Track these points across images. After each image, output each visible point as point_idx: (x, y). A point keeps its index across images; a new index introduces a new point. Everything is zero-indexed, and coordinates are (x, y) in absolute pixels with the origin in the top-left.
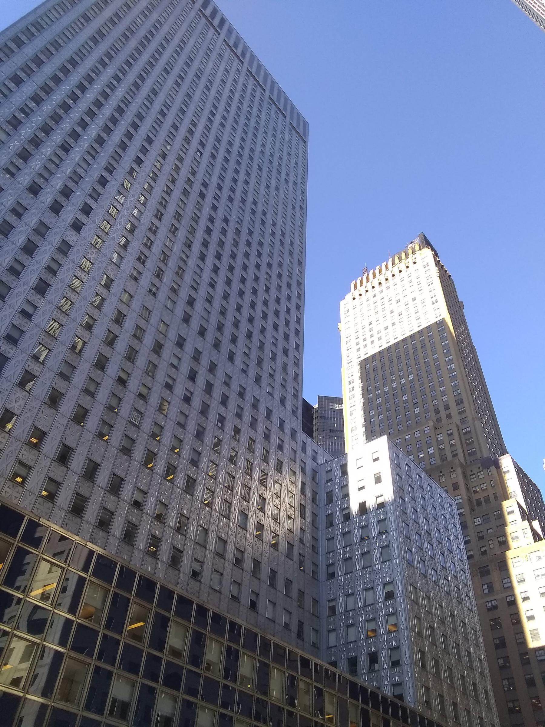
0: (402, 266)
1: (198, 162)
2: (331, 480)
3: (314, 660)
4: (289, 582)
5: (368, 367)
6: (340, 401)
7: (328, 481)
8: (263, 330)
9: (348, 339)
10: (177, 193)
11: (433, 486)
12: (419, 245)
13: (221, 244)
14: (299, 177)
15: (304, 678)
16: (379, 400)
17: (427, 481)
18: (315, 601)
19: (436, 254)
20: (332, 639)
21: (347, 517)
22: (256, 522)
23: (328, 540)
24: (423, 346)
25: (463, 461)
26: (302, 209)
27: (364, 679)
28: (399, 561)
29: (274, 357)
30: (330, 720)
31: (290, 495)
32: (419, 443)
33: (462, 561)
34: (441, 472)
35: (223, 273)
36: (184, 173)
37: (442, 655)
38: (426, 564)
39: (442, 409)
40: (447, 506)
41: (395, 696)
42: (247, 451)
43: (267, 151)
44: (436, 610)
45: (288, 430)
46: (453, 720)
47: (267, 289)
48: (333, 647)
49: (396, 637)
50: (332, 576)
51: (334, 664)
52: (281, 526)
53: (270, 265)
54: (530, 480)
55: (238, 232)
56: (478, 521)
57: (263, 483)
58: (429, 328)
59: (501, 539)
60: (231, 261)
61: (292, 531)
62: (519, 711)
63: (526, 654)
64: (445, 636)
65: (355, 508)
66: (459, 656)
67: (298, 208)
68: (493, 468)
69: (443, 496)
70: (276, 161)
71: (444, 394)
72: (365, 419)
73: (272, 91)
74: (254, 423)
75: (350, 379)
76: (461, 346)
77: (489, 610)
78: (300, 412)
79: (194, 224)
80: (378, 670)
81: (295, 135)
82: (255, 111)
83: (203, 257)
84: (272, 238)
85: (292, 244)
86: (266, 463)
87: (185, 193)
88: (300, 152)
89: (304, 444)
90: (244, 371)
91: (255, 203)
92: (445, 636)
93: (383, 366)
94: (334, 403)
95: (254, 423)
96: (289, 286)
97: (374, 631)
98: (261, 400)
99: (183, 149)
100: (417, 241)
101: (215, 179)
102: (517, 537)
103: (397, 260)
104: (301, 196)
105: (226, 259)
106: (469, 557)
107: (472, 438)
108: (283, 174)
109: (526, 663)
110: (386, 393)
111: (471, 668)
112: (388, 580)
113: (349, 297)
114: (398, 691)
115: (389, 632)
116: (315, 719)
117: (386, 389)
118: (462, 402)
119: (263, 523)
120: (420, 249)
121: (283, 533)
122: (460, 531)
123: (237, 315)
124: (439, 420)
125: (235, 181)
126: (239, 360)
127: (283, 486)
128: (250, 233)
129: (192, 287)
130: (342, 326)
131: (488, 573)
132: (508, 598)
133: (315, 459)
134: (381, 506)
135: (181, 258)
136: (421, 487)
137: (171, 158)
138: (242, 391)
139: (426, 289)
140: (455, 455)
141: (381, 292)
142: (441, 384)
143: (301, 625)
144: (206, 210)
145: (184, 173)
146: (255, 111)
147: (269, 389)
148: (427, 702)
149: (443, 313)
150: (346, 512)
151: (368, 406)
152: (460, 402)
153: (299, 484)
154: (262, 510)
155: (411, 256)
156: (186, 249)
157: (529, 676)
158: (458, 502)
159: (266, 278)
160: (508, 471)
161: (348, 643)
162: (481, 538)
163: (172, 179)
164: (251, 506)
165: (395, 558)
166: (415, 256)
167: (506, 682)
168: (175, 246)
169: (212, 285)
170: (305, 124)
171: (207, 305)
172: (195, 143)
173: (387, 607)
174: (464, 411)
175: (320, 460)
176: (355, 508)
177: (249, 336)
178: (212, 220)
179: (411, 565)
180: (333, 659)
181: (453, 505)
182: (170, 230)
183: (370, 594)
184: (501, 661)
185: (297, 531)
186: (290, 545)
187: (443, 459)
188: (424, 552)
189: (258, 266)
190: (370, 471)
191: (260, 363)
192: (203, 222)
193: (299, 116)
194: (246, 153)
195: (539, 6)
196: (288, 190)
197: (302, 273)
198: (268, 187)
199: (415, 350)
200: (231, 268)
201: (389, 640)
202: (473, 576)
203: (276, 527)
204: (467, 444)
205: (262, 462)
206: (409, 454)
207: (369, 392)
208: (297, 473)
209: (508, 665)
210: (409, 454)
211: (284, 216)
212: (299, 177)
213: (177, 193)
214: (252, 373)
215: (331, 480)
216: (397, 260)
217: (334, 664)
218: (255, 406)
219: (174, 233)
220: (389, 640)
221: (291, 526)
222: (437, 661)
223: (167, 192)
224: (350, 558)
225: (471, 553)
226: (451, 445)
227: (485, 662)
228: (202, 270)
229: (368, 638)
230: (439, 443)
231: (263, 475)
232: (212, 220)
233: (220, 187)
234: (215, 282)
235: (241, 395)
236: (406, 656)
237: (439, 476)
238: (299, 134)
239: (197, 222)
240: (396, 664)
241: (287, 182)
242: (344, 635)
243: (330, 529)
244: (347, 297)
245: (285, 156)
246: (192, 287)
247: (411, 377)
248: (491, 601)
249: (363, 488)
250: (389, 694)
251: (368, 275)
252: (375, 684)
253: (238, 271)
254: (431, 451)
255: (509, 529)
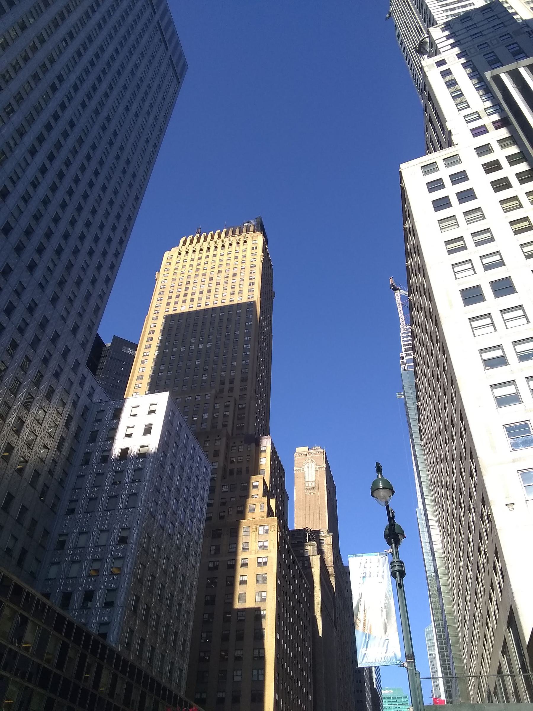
0: (234, 240)
1: (61, 52)
2: (100, 420)
3: (28, 588)
4: (24, 509)
5: (173, 322)
6: (135, 347)
7: (96, 421)
8: (76, 251)
9: (161, 290)
10: (26, 73)
11: (197, 449)
12: (254, 228)
13: (59, 146)
14: (162, 114)
15: (12, 605)
16: (173, 358)
17: (193, 442)
18: (46, 533)
19: (265, 242)
20: (53, 571)
21: (106, 458)
22: (6, 443)
23: (79, 477)
24: (229, 320)
25: (230, 433)
26: (155, 146)
27: (74, 615)
28: (142, 511)
29: (79, 283)
30: (27, 649)
31: (53, 424)
32: (197, 406)
33: (200, 521)
34: (208, 437)
35: (51, 176)
36: (40, 56)
37: (155, 603)
38: (167, 517)
39: (227, 382)
40: (203, 469)
41: (99, 634)
42: (19, 369)
43: (139, 74)
44: (163, 562)
45: (71, 360)
46: (147, 662)
47: (94, 212)
48: (53, 579)
49: (117, 579)
50: (72, 511)
51: (47, 596)
52: (33, 453)
53: (104, 188)
54: (280, 463)
55: (81, 141)
56: (226, 488)
57: (27, 406)
58: (239, 306)
59: (240, 509)
60: (64, 168)
61: (44, 460)
62: (208, 661)
63: (230, 613)
64: (163, 586)
65: (116, 451)
66: (170, 606)
67: (151, 143)
68: (253, 445)
69: (203, 459)
70: (144, 88)
71: (233, 368)
72: (154, 371)
73: (162, 17)
74: (35, 343)
75: (152, 329)
76: (261, 331)
77: (210, 569)
78: (90, 346)
79: (34, 113)
80: (90, 608)
81: (171, 72)
82: (139, 28)
83: (33, 152)
84: (122, 175)
85: (134, 176)
86: (36, 386)
87: (36, 77)
88: (171, 90)
89: (84, 378)
90: (42, 286)
91: (109, 119)
92: (163, 586)
93: (187, 326)
94: (128, 347)
95: (35, 343)
96: (118, 217)
97: (97, 570)
98: (51, 321)
99: (48, 30)
100: (254, 222)
101: (73, 78)
102: (254, 510)
103: (230, 233)
104: (159, 133)
105: (58, 164)
106: (208, 519)
107: (244, 414)
108: (147, 104)
109: (227, 620)
110: (182, 353)
111: (178, 618)
112: (126, 525)
113: (175, 251)
114: (103, 630)
115: (112, 574)
116: (11, 646)
117: (183, 349)
118: (246, 380)
119: (14, 445)
120: (254, 232)
121: (32, 458)
122: (208, 493)
123: (52, 225)
124: (222, 391)
125: (94, 88)
126: (39, 273)
127: (48, 414)
128: (94, 147)
129: (11, 178)
130: (160, 276)
131: (220, 536)
132: (229, 562)
133: (90, 396)
134: (142, 456)
135: (8, 144)
136: (186, 447)
137: (31, 34)
138: (33, 306)
139: (248, 270)
140: (225, 426)
141: (207, 257)
142: (234, 359)
143: (24, 552)
144: (53, 105)
145: (40, 56)
146: (139, 28)
147: (64, 314)
148: (128, 643)
149: (256, 297)
150: (105, 454)
151: (159, 361)
152: (244, 380)
153: (65, 417)
154: (18, 432)
155: (244, 234)
156: (17, 136)
157: (226, 632)
158: (214, 467)
159: (96, 200)
160: (265, 451)
161: (68, 578)
162: (223, 504)
163: (25, 56)
164: (6, 425)
165: (139, 507)
166: (247, 236)
167: (204, 635)
168: (5, 129)
169: (35, 185)
170: (185, 66)
171: (22, 204)
172: (63, 31)
173: (117, 551)
174: (246, 389)
175: (96, 398)
176: (116, 451)
177: (59, 251)
178: (56, 117)
179: (152, 516)
180: (48, 590)
181: (209, 469)
182: (5, 109)
183: (104, 535)
184: (206, 616)
185: (49, 461)
186: (37, 474)
187: (214, 426)
188: (169, 507)
189: (91, 184)
190: (142, 421)
191: (62, 283)
192: (45, 117)
193: (181, 54)
194: (116, 66)
195: (417, 61)
196: (146, 121)
197: (136, 208)
198: (127, 109)
199: (221, 321)
200: (61, 175)
201: (109, 582)
202: (205, 537)
203: (27, 453)
204: (239, 419)
205: (32, 384)
206: (185, 414)
207: (166, 347)
208: (68, 405)
209: (211, 620)
210: (185, 414)
211: (135, 145)
212: (162, 114)
213: (26, 73)
214: (49, 291)
215: (100, 420)
216: (230, 233)
217: (47, 596)
218: (43, 325)
219: (8, 114)
220: (109, 582)
221: (44, 456)
222: (148, 608)
223: (14, 68)
224: (95, 499)
225: (211, 515)
226: (225, 416)
227: (192, 615)
228: (28, 164)
229: (90, 576)
230: (215, 411)
231: (30, 398)
232: (56, 117)
233: (76, 88)
234: (39, 183)
235: (31, 309)
236: (121, 598)
237: (205, 441)
238: (175, 72)
239: (38, 113)
240: (109, 604)
241: (148, 113)
242: (66, 570)
243: (84, 467)
244: (173, 249)
245: (155, 86)
246: (11, 178)
247: (209, 345)
248: (214, 562)
249: (130, 435)
250: (94, 631)
251: (200, 236)
252: (83, 620)
253: (68, 182)
254: (206, 416)
255: (250, 501)
